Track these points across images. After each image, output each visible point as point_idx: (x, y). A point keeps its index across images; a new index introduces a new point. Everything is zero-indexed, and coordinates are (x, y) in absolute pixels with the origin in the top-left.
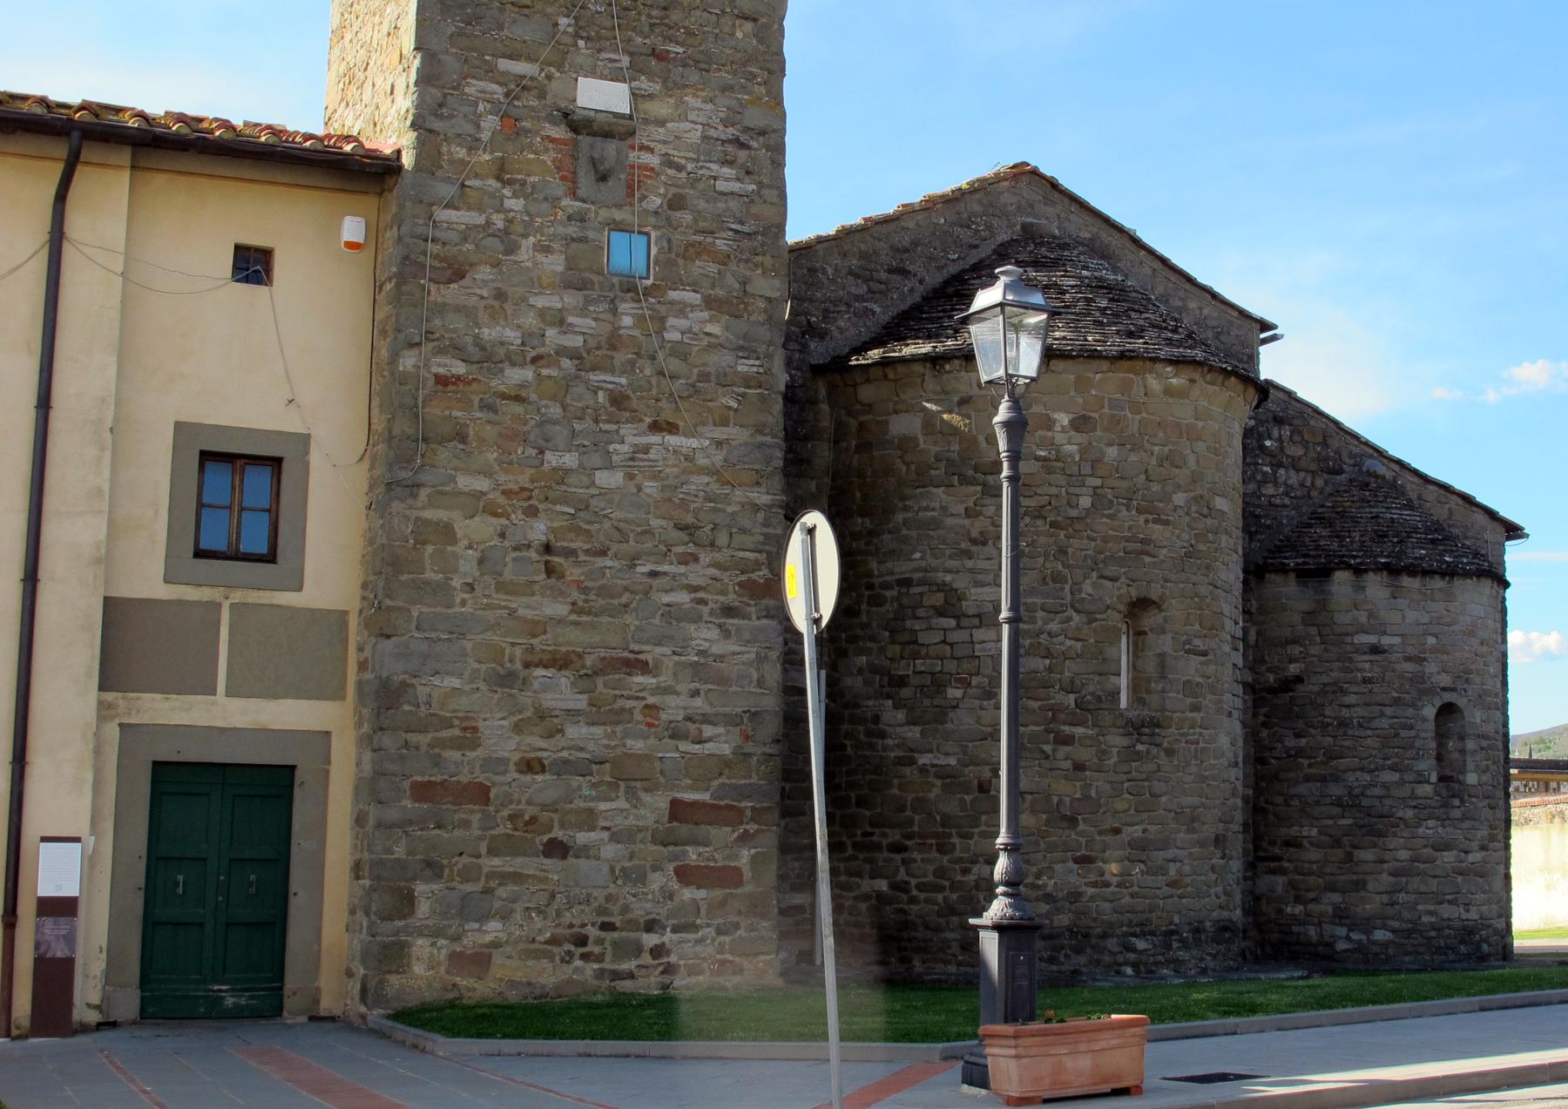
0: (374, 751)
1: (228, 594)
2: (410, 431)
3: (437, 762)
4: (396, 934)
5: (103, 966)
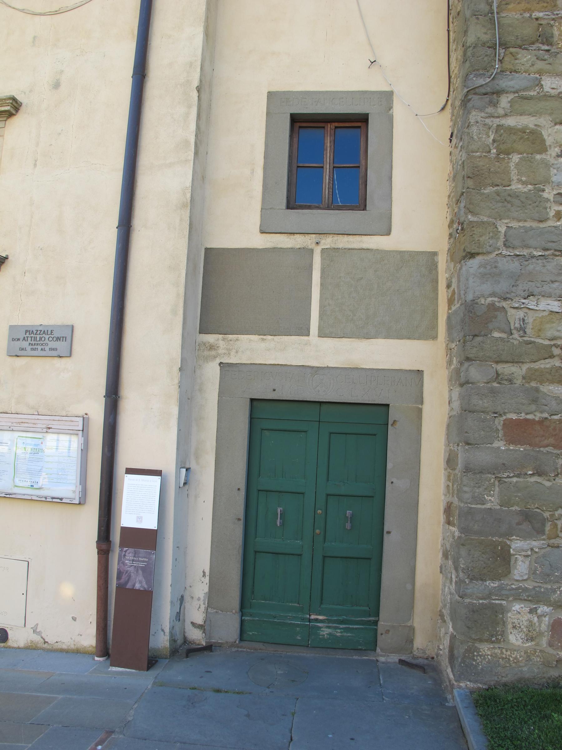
0: (462, 385)
1: (321, 238)
2: (485, 38)
3: (535, 398)
4: (488, 596)
5: (206, 589)
